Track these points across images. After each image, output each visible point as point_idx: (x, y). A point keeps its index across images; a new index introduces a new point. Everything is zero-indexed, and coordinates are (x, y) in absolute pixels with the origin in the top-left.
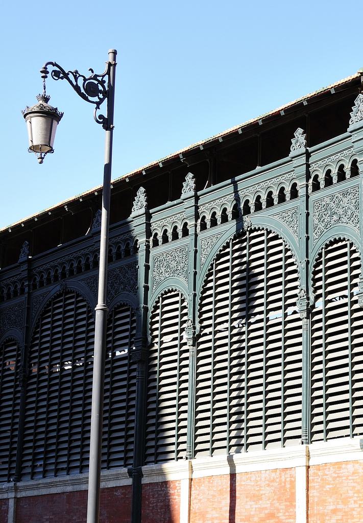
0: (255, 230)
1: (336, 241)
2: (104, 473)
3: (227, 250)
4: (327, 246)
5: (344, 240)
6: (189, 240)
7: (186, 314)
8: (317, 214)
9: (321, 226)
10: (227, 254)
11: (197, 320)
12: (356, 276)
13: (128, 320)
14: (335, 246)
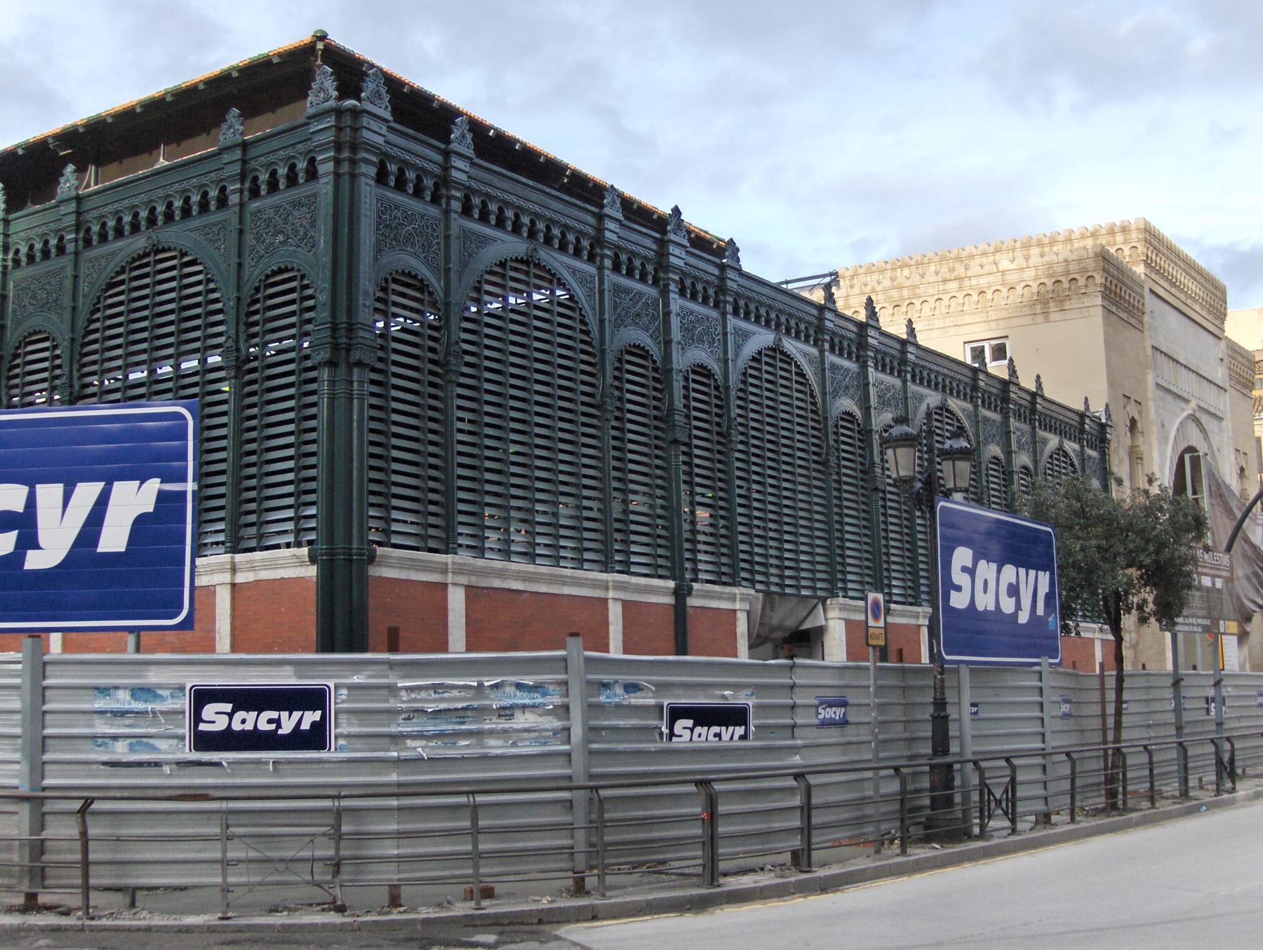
0: (164, 250)
1: (280, 271)
2: (199, 561)
3: (121, 277)
4: (268, 277)
5: (293, 269)
6: (66, 261)
7: (59, 367)
8: (255, 231)
9: (261, 248)
10: (122, 282)
11: (76, 375)
12: (309, 321)
13: (46, 354)
14: (278, 278)
